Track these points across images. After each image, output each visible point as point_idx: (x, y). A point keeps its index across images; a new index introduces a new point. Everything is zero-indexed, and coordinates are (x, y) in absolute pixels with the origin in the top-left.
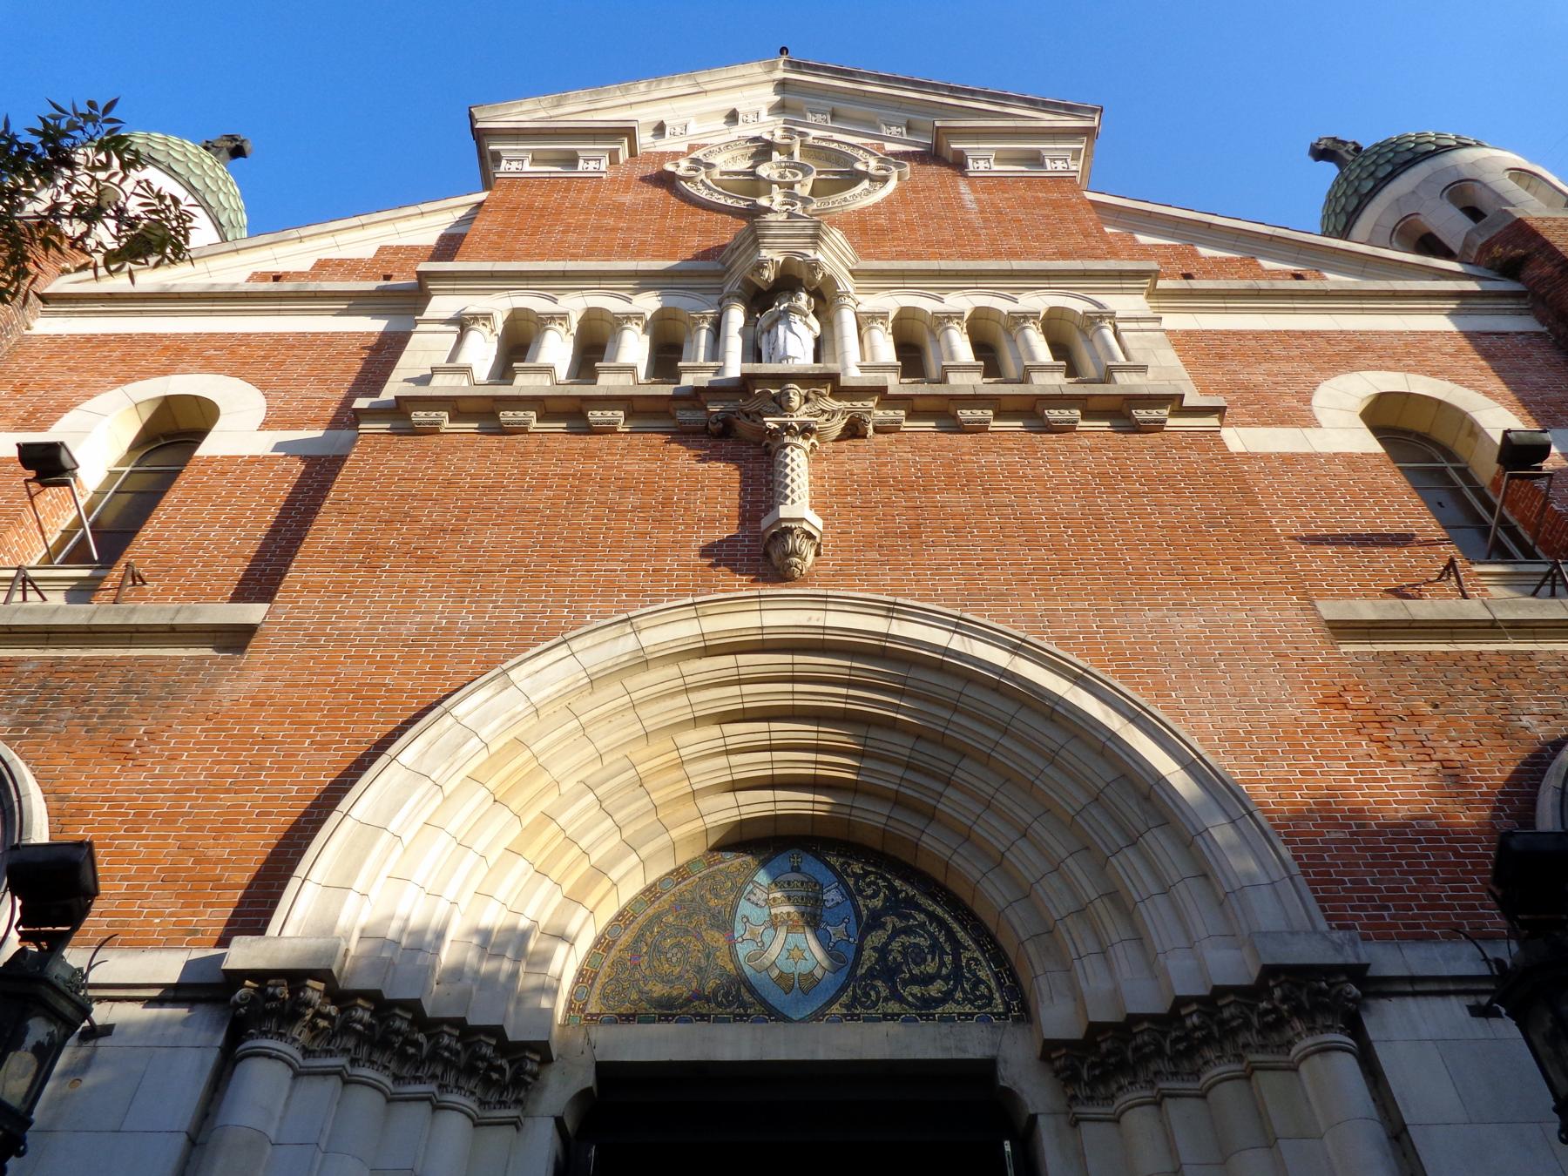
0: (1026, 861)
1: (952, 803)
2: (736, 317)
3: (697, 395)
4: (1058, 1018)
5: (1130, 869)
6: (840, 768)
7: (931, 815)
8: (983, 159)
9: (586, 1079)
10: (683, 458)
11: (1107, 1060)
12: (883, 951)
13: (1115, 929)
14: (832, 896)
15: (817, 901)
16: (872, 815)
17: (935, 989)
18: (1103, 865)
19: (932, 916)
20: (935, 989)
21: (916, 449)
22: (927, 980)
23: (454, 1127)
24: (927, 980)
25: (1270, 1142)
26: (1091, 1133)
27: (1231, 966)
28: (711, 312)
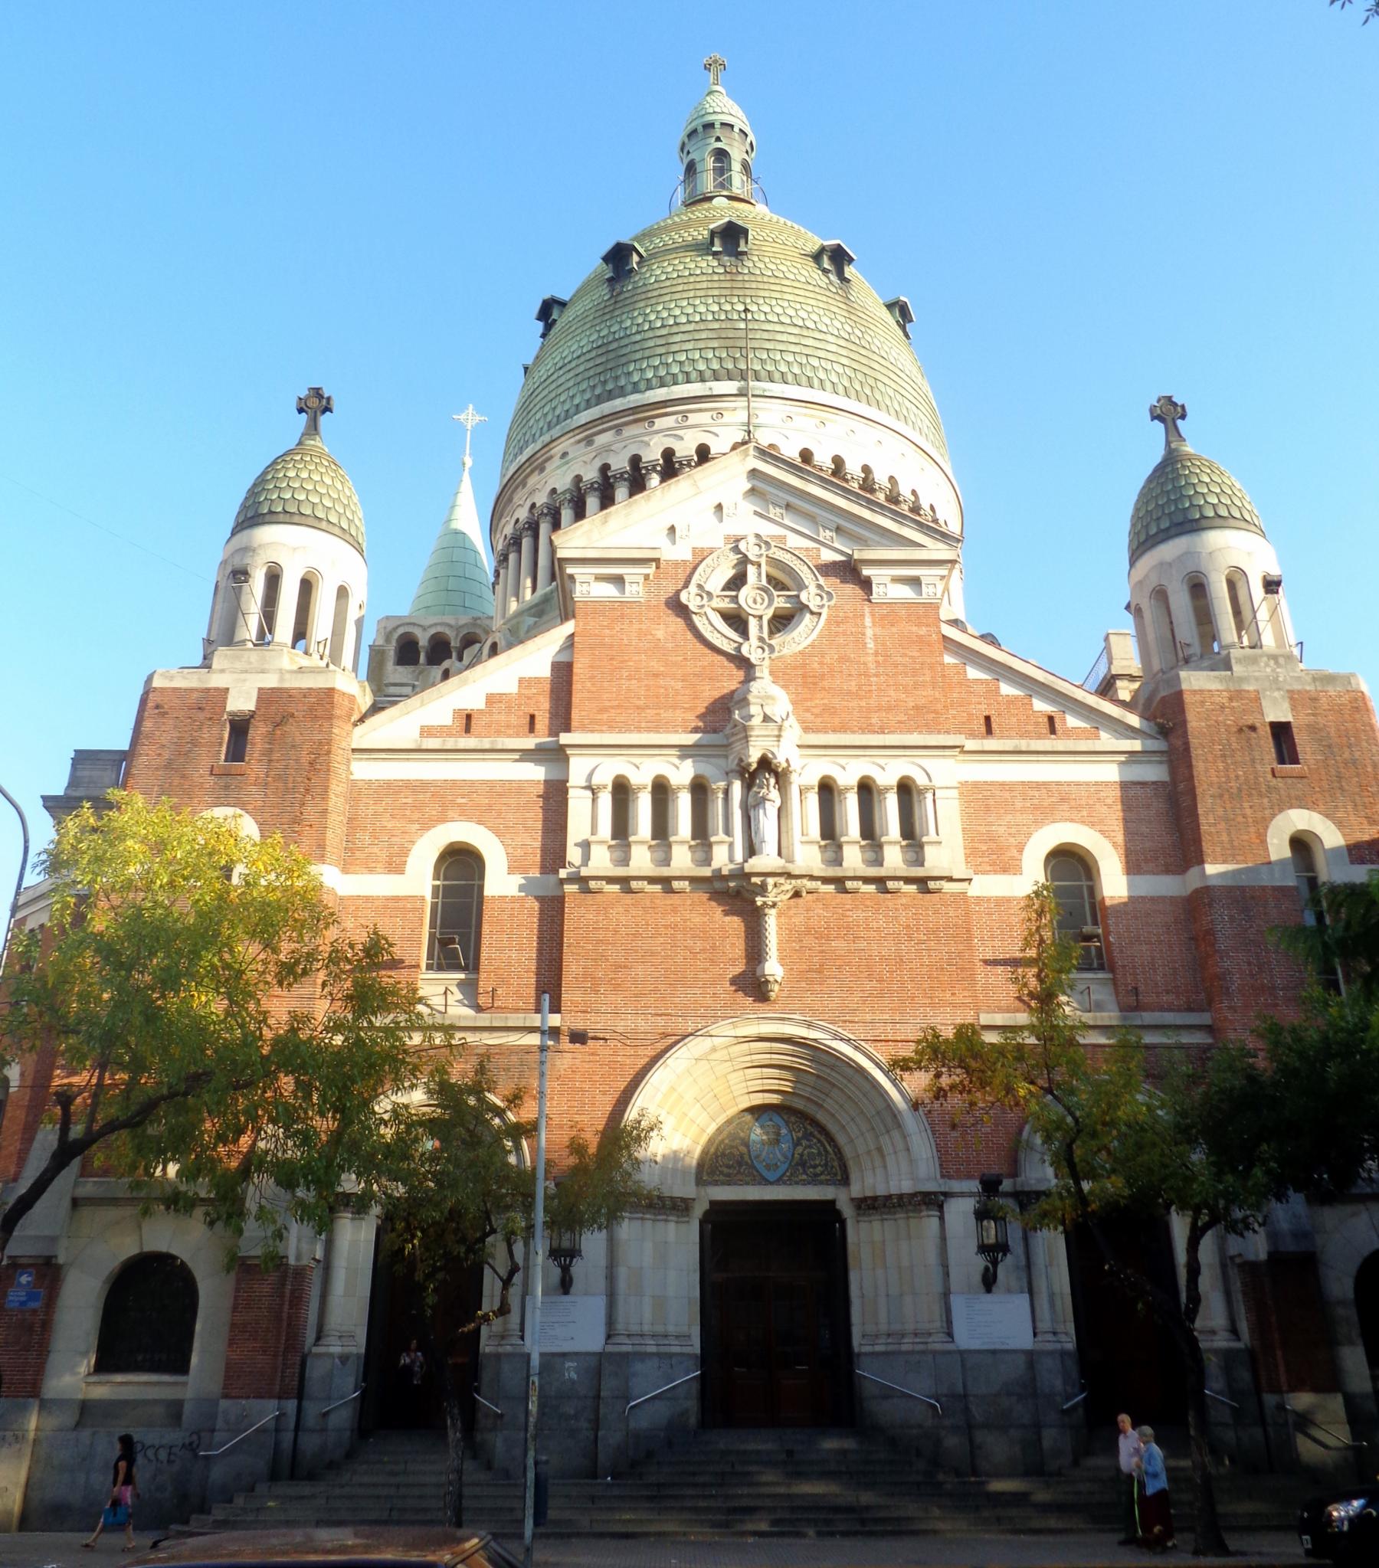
0: (852, 1129)
1: (829, 1104)
2: (737, 787)
3: (718, 876)
4: (856, 1190)
5: (885, 1140)
6: (787, 1087)
7: (821, 1106)
8: (887, 588)
9: (706, 1206)
10: (717, 911)
11: (869, 1205)
12: (801, 1155)
13: (878, 1162)
14: (784, 1131)
15: (778, 1134)
16: (799, 1104)
17: (819, 1169)
18: (877, 1137)
19: (819, 1141)
20: (819, 1169)
21: (826, 907)
22: (815, 1167)
23: (672, 1226)
24: (815, 1167)
25: (909, 1237)
26: (863, 1225)
27: (906, 1187)
28: (722, 784)
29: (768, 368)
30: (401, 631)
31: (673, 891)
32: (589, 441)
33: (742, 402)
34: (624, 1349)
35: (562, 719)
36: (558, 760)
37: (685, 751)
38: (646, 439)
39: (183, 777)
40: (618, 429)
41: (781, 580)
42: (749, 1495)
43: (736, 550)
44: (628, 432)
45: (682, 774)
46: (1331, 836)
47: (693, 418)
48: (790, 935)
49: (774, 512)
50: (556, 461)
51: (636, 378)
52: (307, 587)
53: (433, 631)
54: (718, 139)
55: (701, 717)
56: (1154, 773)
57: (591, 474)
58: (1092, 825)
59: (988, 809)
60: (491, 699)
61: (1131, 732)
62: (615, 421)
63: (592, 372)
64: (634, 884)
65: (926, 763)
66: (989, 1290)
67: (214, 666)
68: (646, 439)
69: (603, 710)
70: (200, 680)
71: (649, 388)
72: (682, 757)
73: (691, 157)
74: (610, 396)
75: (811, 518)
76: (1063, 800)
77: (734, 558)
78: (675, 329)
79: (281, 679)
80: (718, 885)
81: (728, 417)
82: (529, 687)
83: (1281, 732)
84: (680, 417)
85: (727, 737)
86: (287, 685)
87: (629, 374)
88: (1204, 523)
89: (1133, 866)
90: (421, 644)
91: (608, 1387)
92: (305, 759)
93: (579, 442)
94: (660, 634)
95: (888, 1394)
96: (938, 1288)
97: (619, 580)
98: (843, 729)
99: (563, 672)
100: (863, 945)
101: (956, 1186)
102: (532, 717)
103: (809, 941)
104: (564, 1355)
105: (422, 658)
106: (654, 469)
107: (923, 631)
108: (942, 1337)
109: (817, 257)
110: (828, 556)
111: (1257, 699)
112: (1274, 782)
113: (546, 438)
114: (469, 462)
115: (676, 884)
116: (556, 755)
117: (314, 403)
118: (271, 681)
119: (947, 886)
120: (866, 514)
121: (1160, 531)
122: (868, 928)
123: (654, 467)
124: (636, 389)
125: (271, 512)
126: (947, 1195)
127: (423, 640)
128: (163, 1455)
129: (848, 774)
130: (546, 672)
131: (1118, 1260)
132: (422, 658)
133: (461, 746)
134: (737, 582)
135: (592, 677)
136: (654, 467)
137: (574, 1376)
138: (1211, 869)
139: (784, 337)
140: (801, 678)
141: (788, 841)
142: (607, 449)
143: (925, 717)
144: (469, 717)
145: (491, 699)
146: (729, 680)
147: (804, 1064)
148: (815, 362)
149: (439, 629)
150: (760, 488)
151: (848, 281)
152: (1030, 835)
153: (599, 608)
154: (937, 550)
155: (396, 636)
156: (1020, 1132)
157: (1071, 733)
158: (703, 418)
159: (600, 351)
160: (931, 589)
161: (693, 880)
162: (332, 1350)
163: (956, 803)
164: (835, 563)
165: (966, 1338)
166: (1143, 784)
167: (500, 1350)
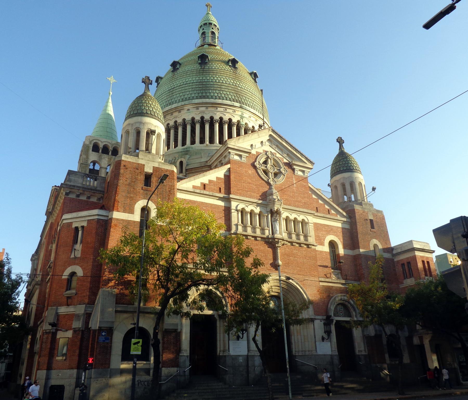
21: (288, 249)
30: (95, 141)
31: (257, 240)
32: (197, 108)
33: (240, 109)
34: (253, 354)
35: (228, 190)
36: (227, 201)
37: (258, 205)
38: (225, 113)
39: (134, 188)
40: (207, 107)
41: (276, 164)
43: (266, 154)
44: (210, 109)
45: (257, 210)
46: (380, 247)
47: (228, 110)
48: (282, 255)
49: (274, 146)
50: (185, 111)
51: (212, 94)
53: (104, 143)
54: (213, 28)
55: (260, 196)
56: (347, 226)
57: (198, 118)
58: (337, 236)
59: (318, 229)
60: (210, 181)
61: (344, 216)
62: (207, 105)
63: (198, 89)
64: (249, 237)
65: (308, 217)
66: (238, 340)
67: (140, 157)
68: (225, 113)
69: (238, 190)
70: (136, 160)
71: (216, 99)
72: (257, 206)
73: (204, 31)
74: (204, 97)
75: (281, 150)
76: (332, 230)
77: (266, 156)
78: (215, 83)
79: (159, 165)
80: (267, 240)
81: (237, 113)
82: (219, 180)
83: (371, 221)
85: (268, 203)
86: (161, 167)
87: (210, 93)
88: (354, 170)
89: (344, 248)
90: (110, 148)
91: (250, 363)
92: (167, 190)
93: (194, 107)
94: (250, 172)
95: (303, 364)
96: (314, 341)
97: (240, 156)
98: (290, 205)
99: (227, 178)
100: (296, 259)
101: (317, 317)
102: (220, 188)
103: (286, 256)
104: (239, 356)
105: (110, 153)
106: (218, 121)
107: (305, 184)
108: (315, 352)
110: (285, 161)
111: (367, 213)
112: (371, 233)
113: (183, 103)
114: (111, 93)
115: (258, 238)
116: (227, 200)
117: (147, 81)
118: (156, 165)
119: (313, 247)
120: (295, 152)
121: (343, 170)
122: (297, 255)
124: (212, 98)
125: (147, 113)
126: (315, 319)
127: (101, 146)
128: (146, 383)
129: (292, 217)
130: (222, 176)
131: (344, 335)
132: (110, 153)
133: (205, 193)
134: (265, 162)
135: (235, 181)
137: (241, 361)
138: (361, 250)
139: (248, 95)
140: (281, 190)
141: (281, 232)
142: (203, 112)
143: (306, 205)
144: (204, 185)
145: (210, 181)
146: (266, 188)
147: (284, 286)
148: (255, 103)
149: (106, 143)
150: (271, 140)
152: (326, 237)
153: (236, 162)
154: (309, 165)
155: (93, 143)
156: (328, 306)
157: (333, 214)
158: (222, 109)
159: (200, 84)
160: (306, 174)
161: (262, 238)
162: (185, 354)
164: (287, 163)
165: (320, 352)
166: (345, 228)
167: (225, 354)
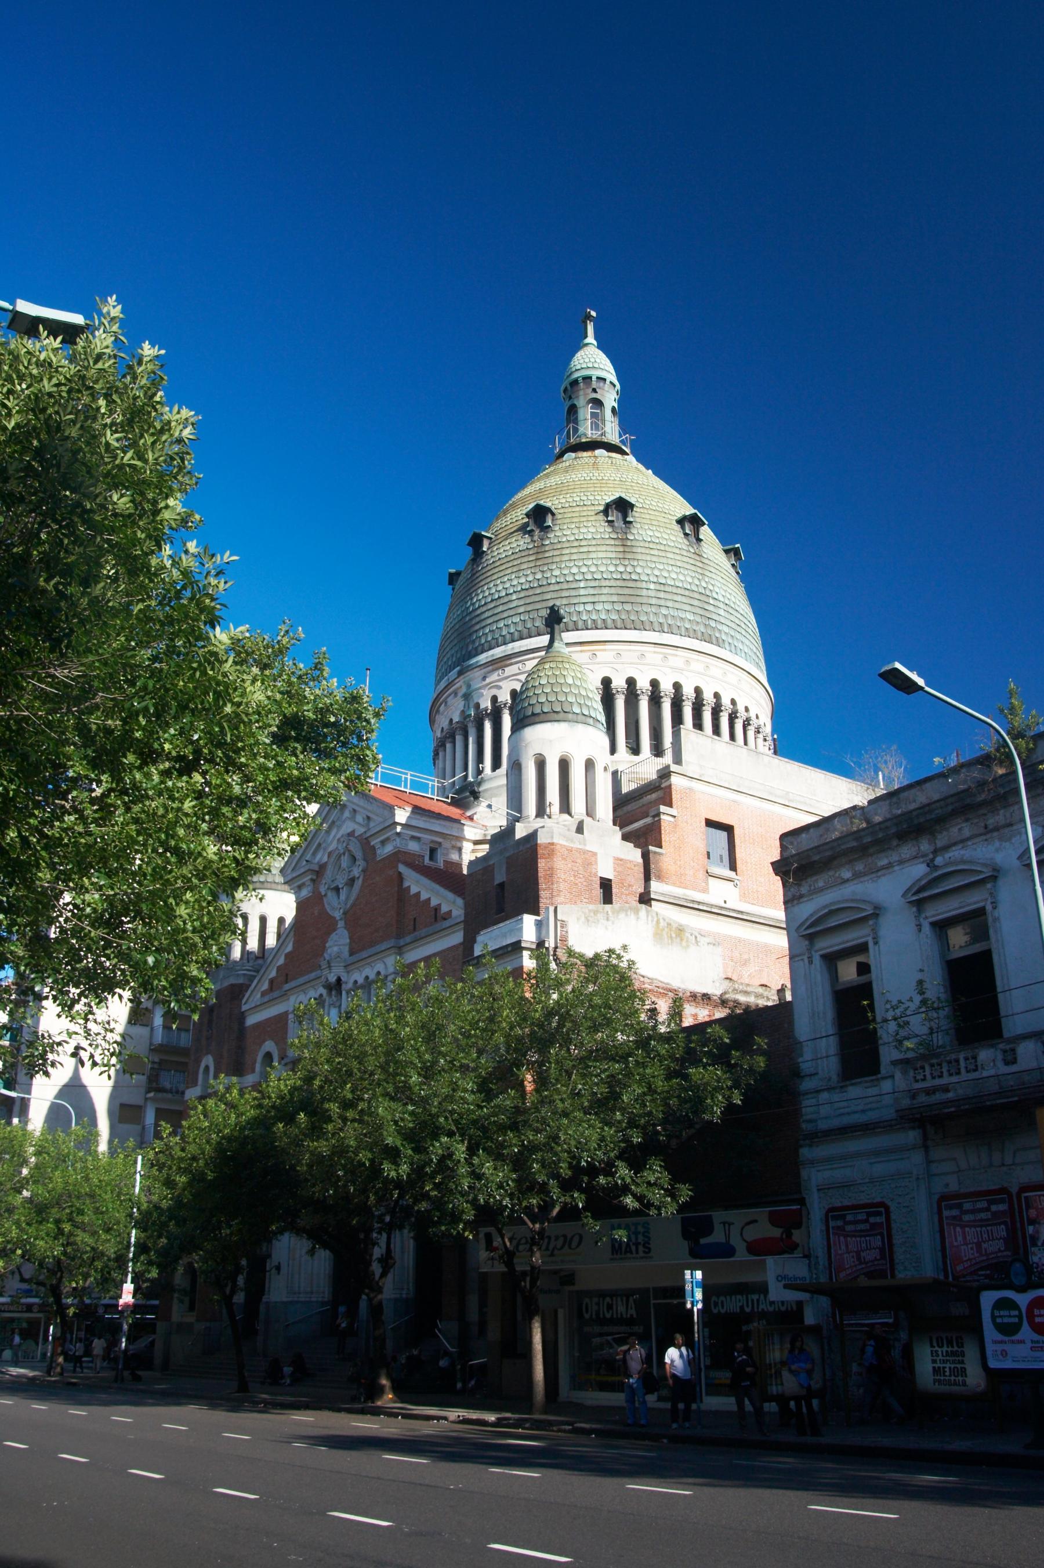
29: (623, 617)
42: (857, 1325)
52: (564, 765)
84: (520, 665)
109: (681, 522)
123: (505, 704)
125: (533, 714)
136: (505, 704)
148: (664, 611)
151: (701, 540)
163: (780, 941)
